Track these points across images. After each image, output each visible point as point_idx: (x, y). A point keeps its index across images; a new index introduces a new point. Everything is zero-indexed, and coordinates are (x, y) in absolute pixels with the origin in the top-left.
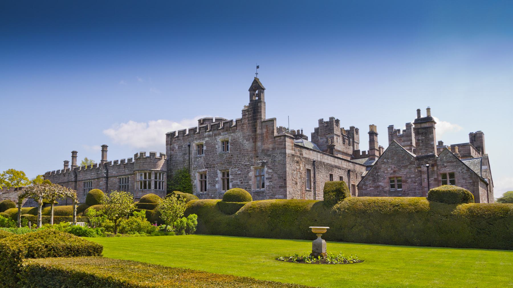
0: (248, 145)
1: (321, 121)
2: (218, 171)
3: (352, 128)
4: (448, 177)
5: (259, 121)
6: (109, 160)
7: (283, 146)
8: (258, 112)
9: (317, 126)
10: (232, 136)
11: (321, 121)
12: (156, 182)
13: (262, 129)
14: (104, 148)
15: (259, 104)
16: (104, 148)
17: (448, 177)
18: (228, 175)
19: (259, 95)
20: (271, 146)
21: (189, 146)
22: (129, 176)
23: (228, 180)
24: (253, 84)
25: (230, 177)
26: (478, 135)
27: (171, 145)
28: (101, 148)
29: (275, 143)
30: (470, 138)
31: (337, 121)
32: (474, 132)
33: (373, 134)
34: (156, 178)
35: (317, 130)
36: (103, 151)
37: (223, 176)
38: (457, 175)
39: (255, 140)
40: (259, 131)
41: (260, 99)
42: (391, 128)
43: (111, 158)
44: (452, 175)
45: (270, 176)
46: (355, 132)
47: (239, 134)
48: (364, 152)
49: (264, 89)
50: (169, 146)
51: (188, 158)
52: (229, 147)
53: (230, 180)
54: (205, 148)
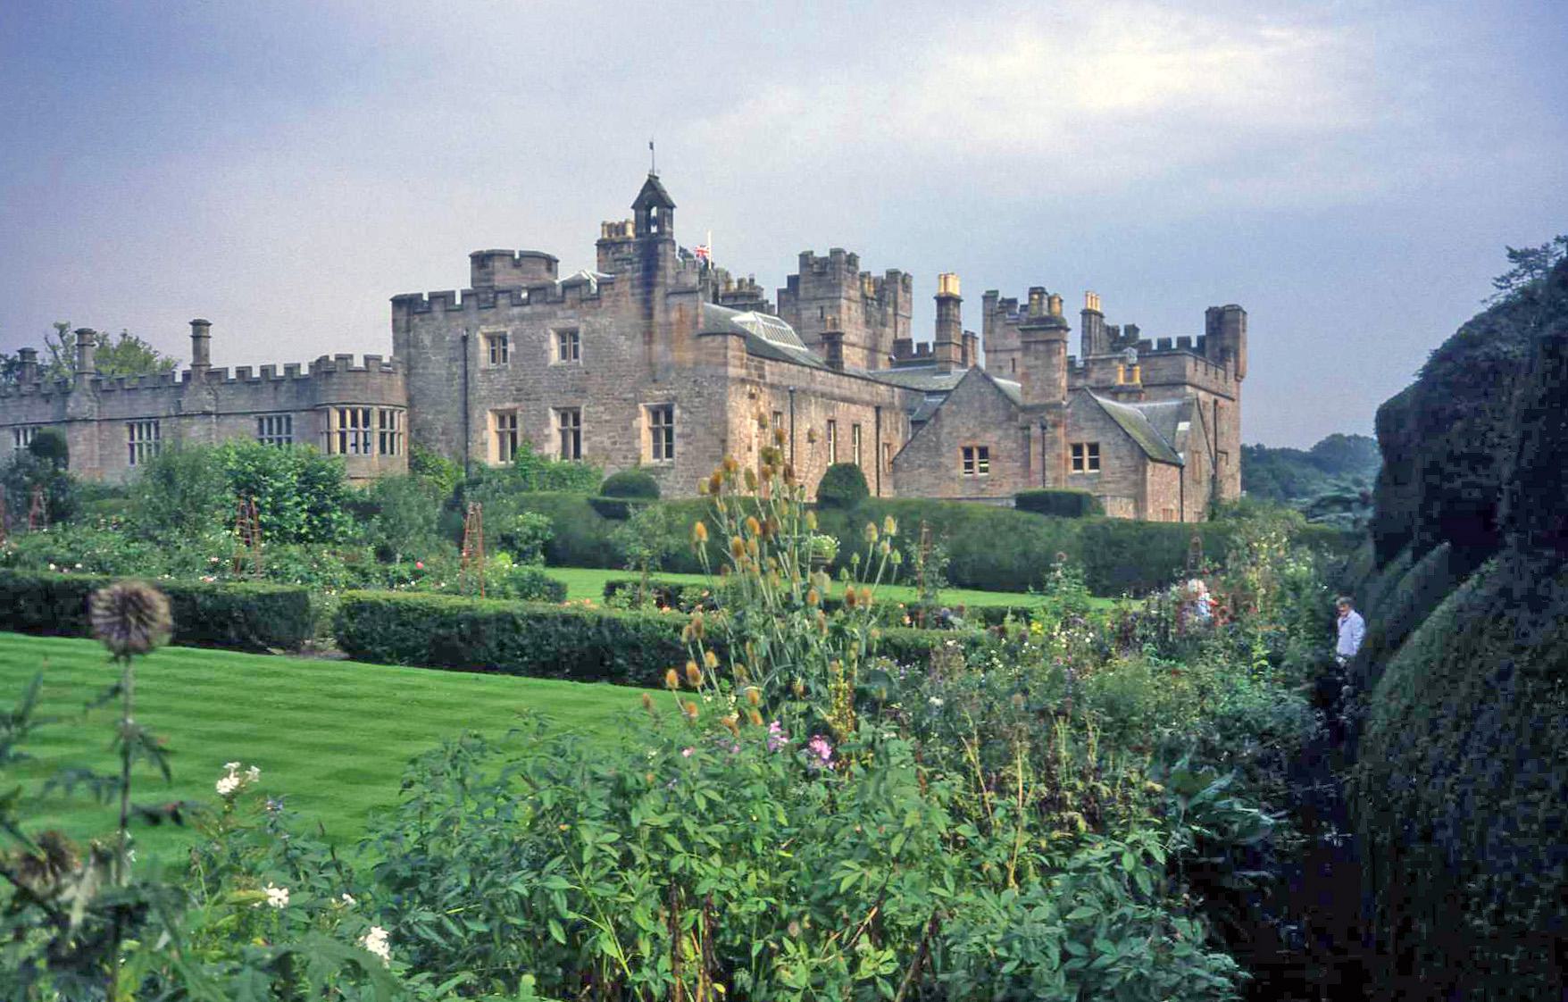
0: (630, 348)
1: (805, 258)
2: (552, 412)
3: (893, 274)
4: (1086, 451)
5: (659, 293)
6: (215, 363)
7: (721, 359)
8: (657, 267)
9: (795, 270)
10: (589, 324)
11: (805, 258)
12: (383, 435)
13: (667, 311)
14: (200, 329)
15: (660, 247)
16: (200, 329)
17: (1086, 451)
18: (577, 422)
19: (658, 222)
20: (689, 356)
21: (465, 339)
22: (293, 415)
23: (577, 435)
24: (643, 191)
25: (584, 427)
26: (1228, 316)
27: (408, 331)
28: (190, 330)
29: (699, 349)
30: (1208, 323)
31: (852, 260)
32: (1220, 305)
33: (946, 302)
34: (383, 425)
35: (793, 281)
36: (197, 337)
37: (564, 422)
38: (1103, 448)
39: (649, 336)
40: (659, 317)
41: (661, 232)
42: (990, 297)
43: (226, 355)
44: (1094, 449)
45: (688, 430)
46: (900, 287)
47: (605, 321)
48: (923, 347)
49: (672, 207)
50: (403, 337)
51: (460, 372)
52: (581, 349)
53: (582, 435)
54: (511, 347)
